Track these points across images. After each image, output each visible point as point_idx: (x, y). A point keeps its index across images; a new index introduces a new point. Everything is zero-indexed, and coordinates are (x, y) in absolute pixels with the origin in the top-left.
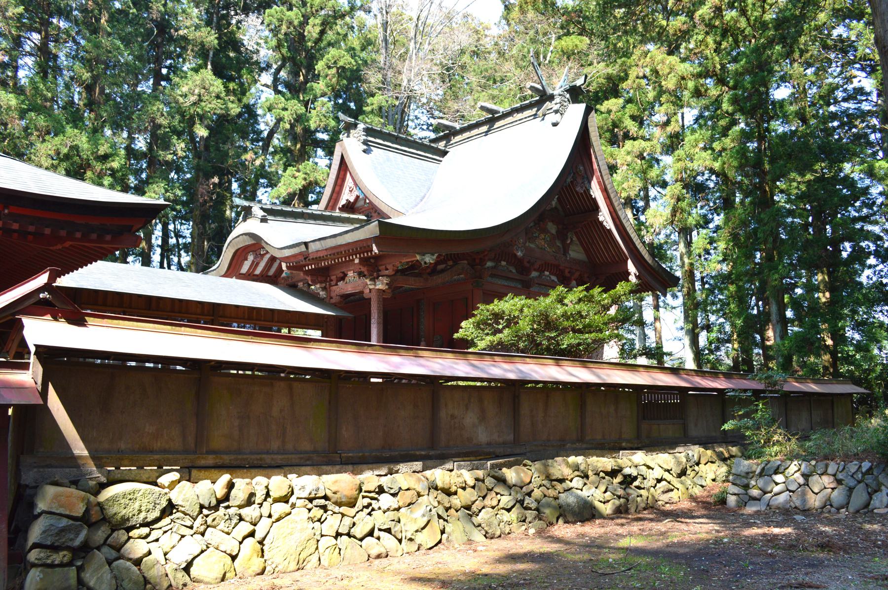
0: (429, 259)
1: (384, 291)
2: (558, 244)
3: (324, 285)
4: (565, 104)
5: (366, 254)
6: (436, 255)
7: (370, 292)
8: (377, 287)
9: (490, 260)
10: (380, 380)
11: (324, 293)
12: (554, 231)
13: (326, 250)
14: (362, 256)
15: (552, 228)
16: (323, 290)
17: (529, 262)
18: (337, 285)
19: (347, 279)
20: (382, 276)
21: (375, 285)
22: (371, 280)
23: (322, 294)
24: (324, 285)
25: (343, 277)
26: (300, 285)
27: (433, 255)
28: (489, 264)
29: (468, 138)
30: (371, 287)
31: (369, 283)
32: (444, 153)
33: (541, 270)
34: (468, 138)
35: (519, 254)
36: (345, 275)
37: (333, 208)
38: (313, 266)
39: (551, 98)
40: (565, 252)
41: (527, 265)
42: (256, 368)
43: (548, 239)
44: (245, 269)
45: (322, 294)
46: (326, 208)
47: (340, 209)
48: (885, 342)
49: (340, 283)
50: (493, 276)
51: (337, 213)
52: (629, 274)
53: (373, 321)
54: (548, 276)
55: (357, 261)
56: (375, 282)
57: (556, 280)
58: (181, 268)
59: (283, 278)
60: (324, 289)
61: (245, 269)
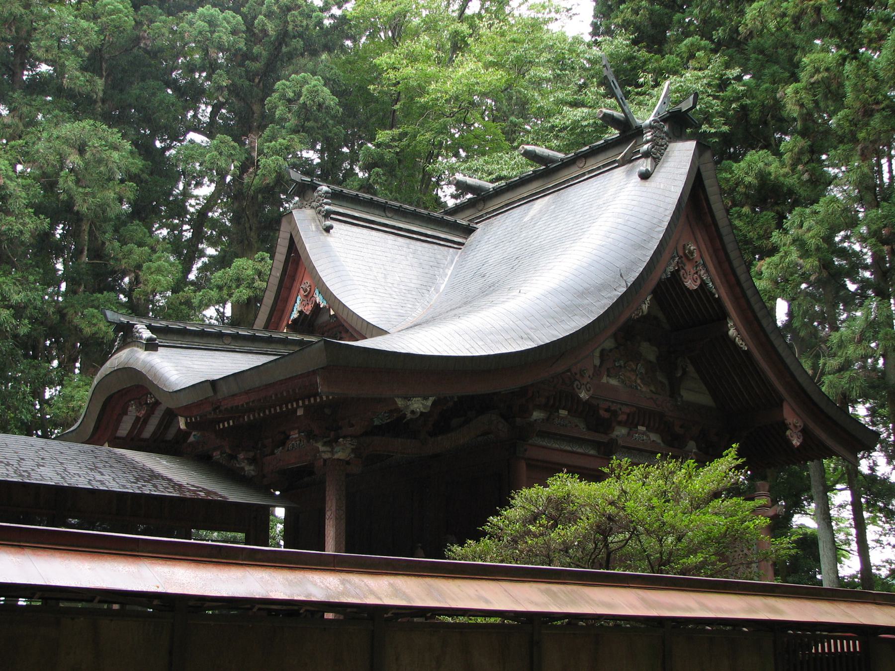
0: (418, 405)
1: (348, 463)
2: (661, 377)
3: (251, 454)
4: (661, 142)
5: (312, 400)
6: (431, 399)
7: (325, 464)
8: (336, 456)
9: (539, 407)
10: (857, 642)
11: (252, 467)
12: (652, 357)
13: (247, 393)
14: (307, 403)
15: (649, 352)
16: (250, 464)
17: (608, 410)
18: (273, 453)
19: (290, 444)
20: (345, 437)
21: (332, 452)
22: (325, 444)
23: (249, 469)
24: (251, 454)
25: (283, 442)
26: (216, 455)
27: (426, 398)
28: (537, 415)
29: (507, 205)
30: (326, 456)
31: (321, 448)
32: (468, 231)
33: (631, 424)
34: (507, 205)
35: (583, 395)
36: (288, 437)
37: (277, 328)
38: (231, 422)
39: (639, 132)
40: (674, 392)
41: (606, 415)
42: (98, 598)
43: (643, 371)
44: (124, 429)
45: (249, 469)
46: (266, 327)
47: (288, 326)
48: (104, 2)
49: (278, 451)
50: (543, 434)
51: (284, 332)
52: (785, 427)
53: (328, 514)
54: (644, 433)
55: (300, 412)
56: (333, 449)
57: (659, 441)
58: (38, 436)
59: (191, 443)
60: (253, 461)
61: (124, 429)
